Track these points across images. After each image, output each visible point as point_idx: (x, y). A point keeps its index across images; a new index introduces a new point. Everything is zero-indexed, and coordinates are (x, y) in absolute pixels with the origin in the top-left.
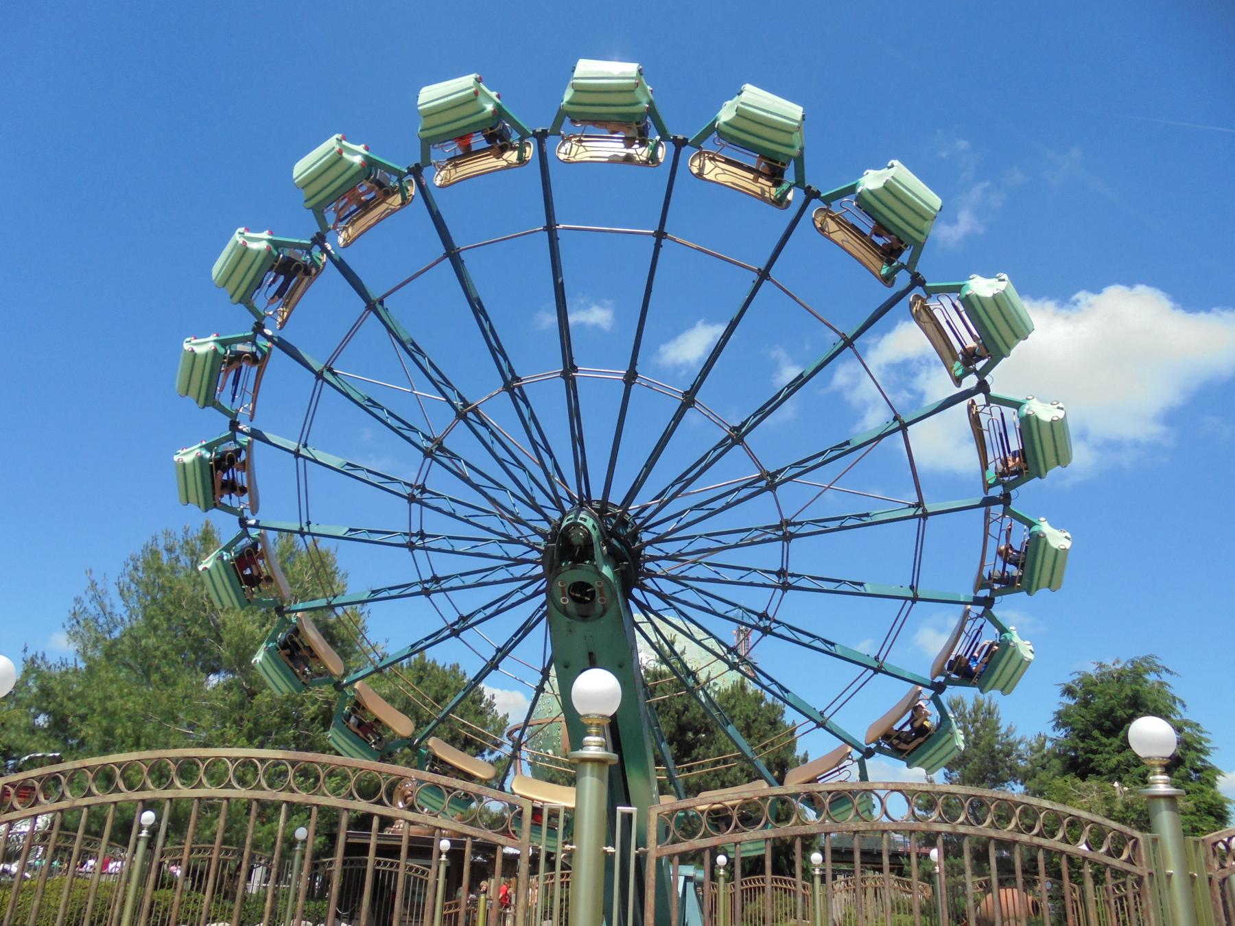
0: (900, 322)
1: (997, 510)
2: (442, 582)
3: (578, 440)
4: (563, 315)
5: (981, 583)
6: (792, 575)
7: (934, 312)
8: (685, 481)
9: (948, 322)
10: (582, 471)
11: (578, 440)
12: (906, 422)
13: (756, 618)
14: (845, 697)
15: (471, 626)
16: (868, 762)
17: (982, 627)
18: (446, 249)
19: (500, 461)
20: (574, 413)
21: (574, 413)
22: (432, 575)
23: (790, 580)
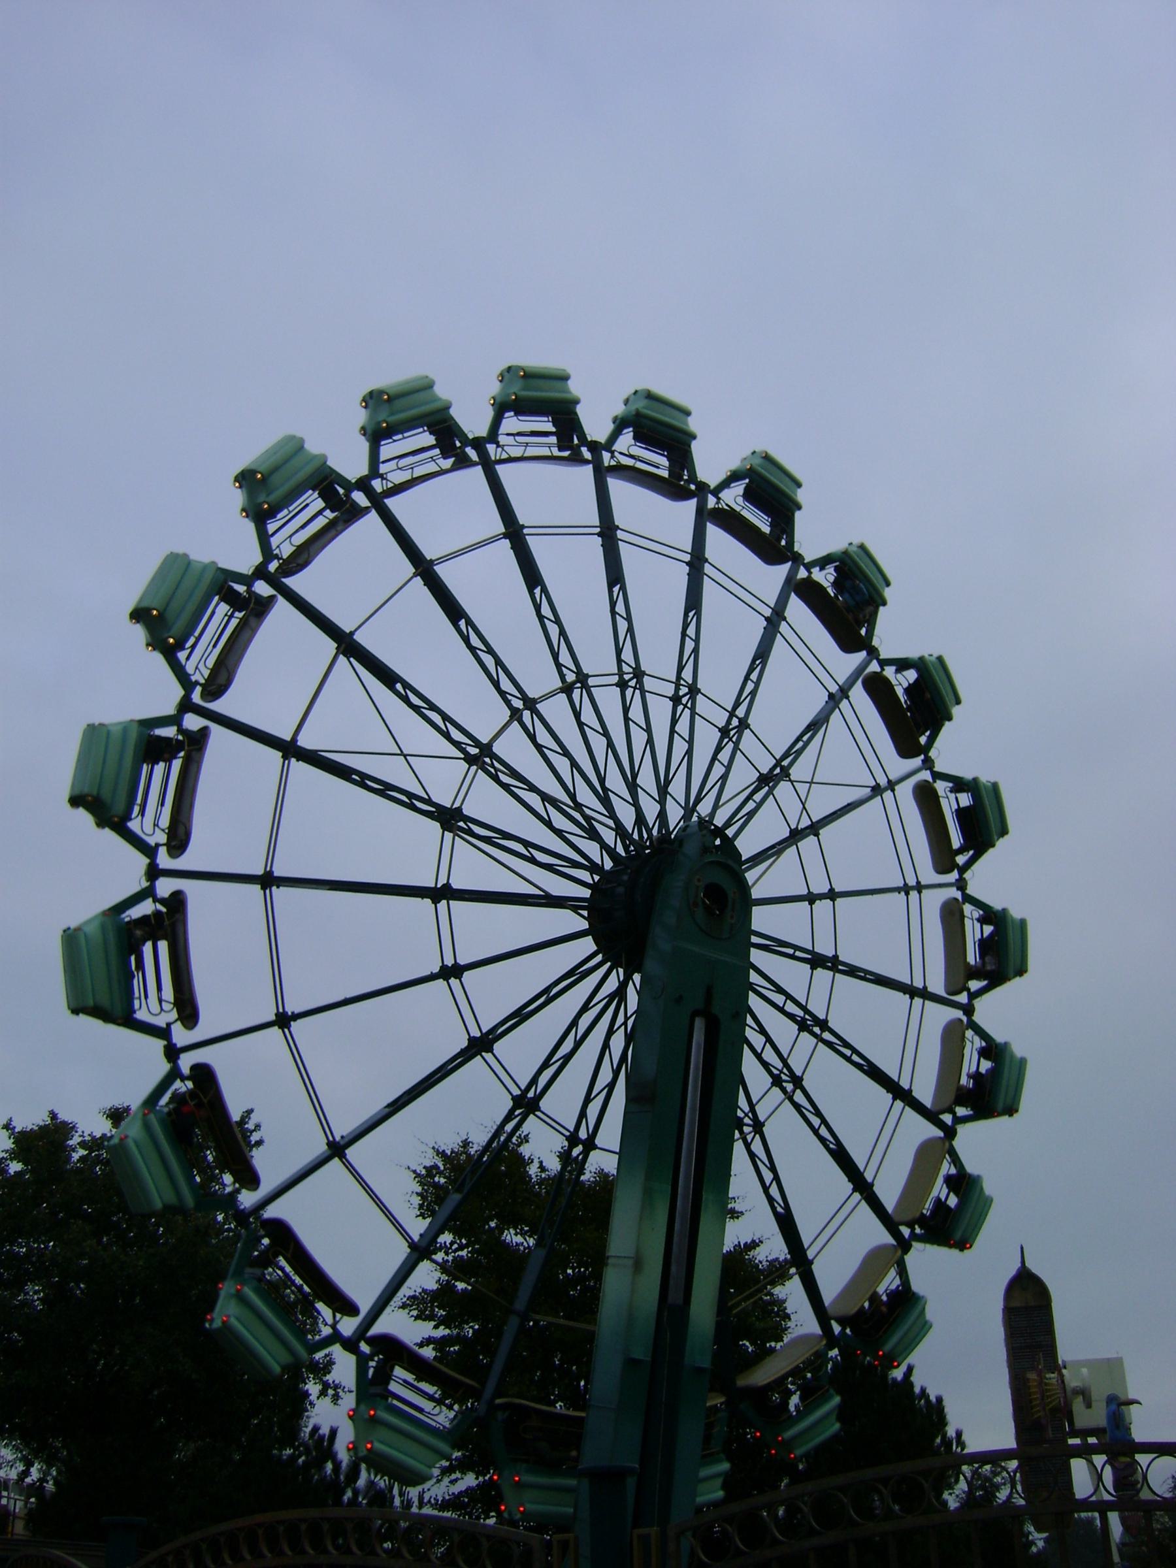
0: (605, 1269)
1: (377, 485)
2: (776, 1072)
3: (548, 996)
4: (232, 640)
5: (462, 462)
6: (562, 677)
7: (211, 667)
8: (529, 851)
9: (215, 646)
10: (576, 974)
11: (548, 996)
12: (179, 1045)
13: (629, 692)
14: (655, 547)
15: (804, 1008)
16: (713, 484)
17: (508, 434)
18: (279, 750)
19: (578, 1044)
20: (521, 1015)
21: (521, 1015)
22: (774, 1087)
23: (571, 677)
